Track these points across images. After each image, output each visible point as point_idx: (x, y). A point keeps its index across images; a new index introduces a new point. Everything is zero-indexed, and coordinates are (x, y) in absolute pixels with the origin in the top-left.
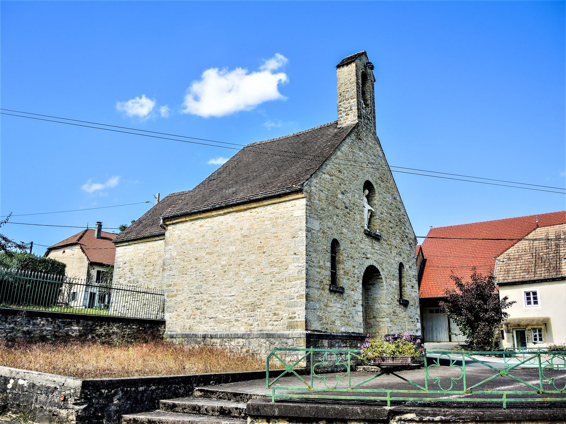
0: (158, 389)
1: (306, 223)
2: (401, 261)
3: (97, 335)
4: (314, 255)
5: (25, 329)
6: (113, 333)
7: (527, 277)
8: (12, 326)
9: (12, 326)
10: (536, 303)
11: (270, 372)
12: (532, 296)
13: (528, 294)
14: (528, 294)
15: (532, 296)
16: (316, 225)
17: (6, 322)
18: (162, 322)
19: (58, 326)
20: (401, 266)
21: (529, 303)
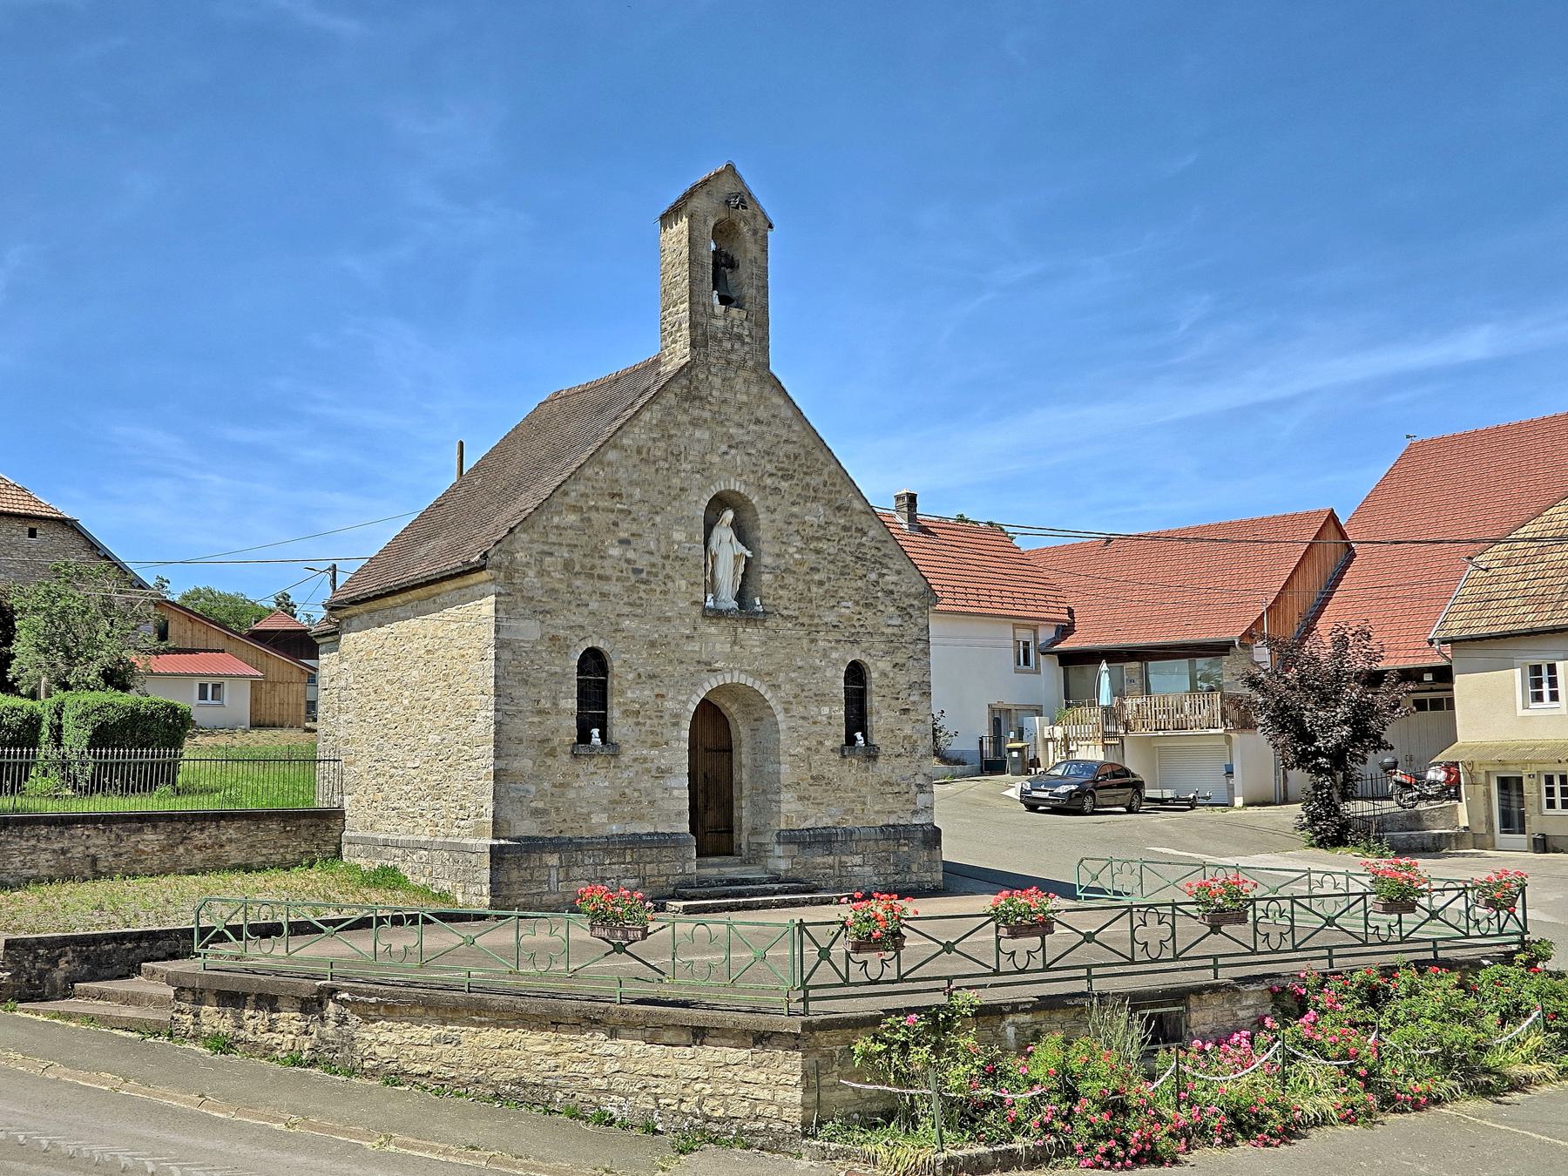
0: (138, 947)
1: (496, 632)
2: (857, 655)
3: (196, 847)
4: (519, 692)
5: (56, 846)
6: (230, 841)
7: (1533, 620)
8: (33, 842)
9: (33, 842)
10: (1554, 696)
11: (291, 925)
12: (1545, 675)
13: (1536, 670)
14: (1536, 670)
15: (1545, 675)
16: (529, 630)
17: (21, 837)
18: (337, 814)
19: (118, 836)
20: (856, 673)
21: (1538, 697)
